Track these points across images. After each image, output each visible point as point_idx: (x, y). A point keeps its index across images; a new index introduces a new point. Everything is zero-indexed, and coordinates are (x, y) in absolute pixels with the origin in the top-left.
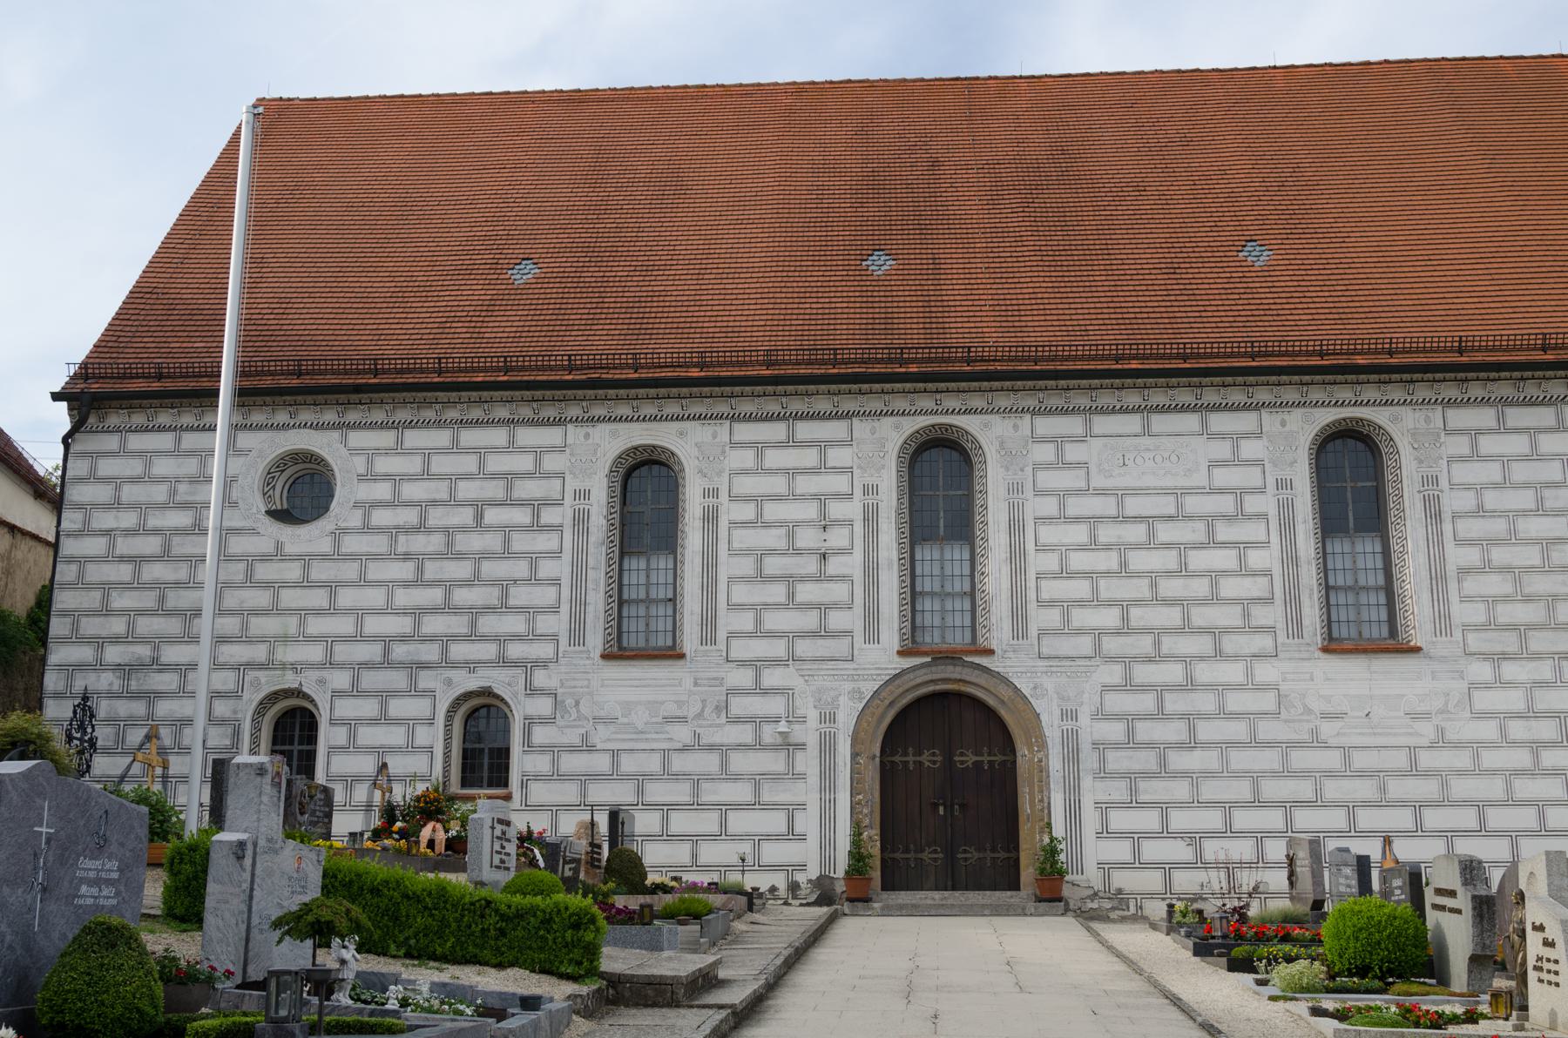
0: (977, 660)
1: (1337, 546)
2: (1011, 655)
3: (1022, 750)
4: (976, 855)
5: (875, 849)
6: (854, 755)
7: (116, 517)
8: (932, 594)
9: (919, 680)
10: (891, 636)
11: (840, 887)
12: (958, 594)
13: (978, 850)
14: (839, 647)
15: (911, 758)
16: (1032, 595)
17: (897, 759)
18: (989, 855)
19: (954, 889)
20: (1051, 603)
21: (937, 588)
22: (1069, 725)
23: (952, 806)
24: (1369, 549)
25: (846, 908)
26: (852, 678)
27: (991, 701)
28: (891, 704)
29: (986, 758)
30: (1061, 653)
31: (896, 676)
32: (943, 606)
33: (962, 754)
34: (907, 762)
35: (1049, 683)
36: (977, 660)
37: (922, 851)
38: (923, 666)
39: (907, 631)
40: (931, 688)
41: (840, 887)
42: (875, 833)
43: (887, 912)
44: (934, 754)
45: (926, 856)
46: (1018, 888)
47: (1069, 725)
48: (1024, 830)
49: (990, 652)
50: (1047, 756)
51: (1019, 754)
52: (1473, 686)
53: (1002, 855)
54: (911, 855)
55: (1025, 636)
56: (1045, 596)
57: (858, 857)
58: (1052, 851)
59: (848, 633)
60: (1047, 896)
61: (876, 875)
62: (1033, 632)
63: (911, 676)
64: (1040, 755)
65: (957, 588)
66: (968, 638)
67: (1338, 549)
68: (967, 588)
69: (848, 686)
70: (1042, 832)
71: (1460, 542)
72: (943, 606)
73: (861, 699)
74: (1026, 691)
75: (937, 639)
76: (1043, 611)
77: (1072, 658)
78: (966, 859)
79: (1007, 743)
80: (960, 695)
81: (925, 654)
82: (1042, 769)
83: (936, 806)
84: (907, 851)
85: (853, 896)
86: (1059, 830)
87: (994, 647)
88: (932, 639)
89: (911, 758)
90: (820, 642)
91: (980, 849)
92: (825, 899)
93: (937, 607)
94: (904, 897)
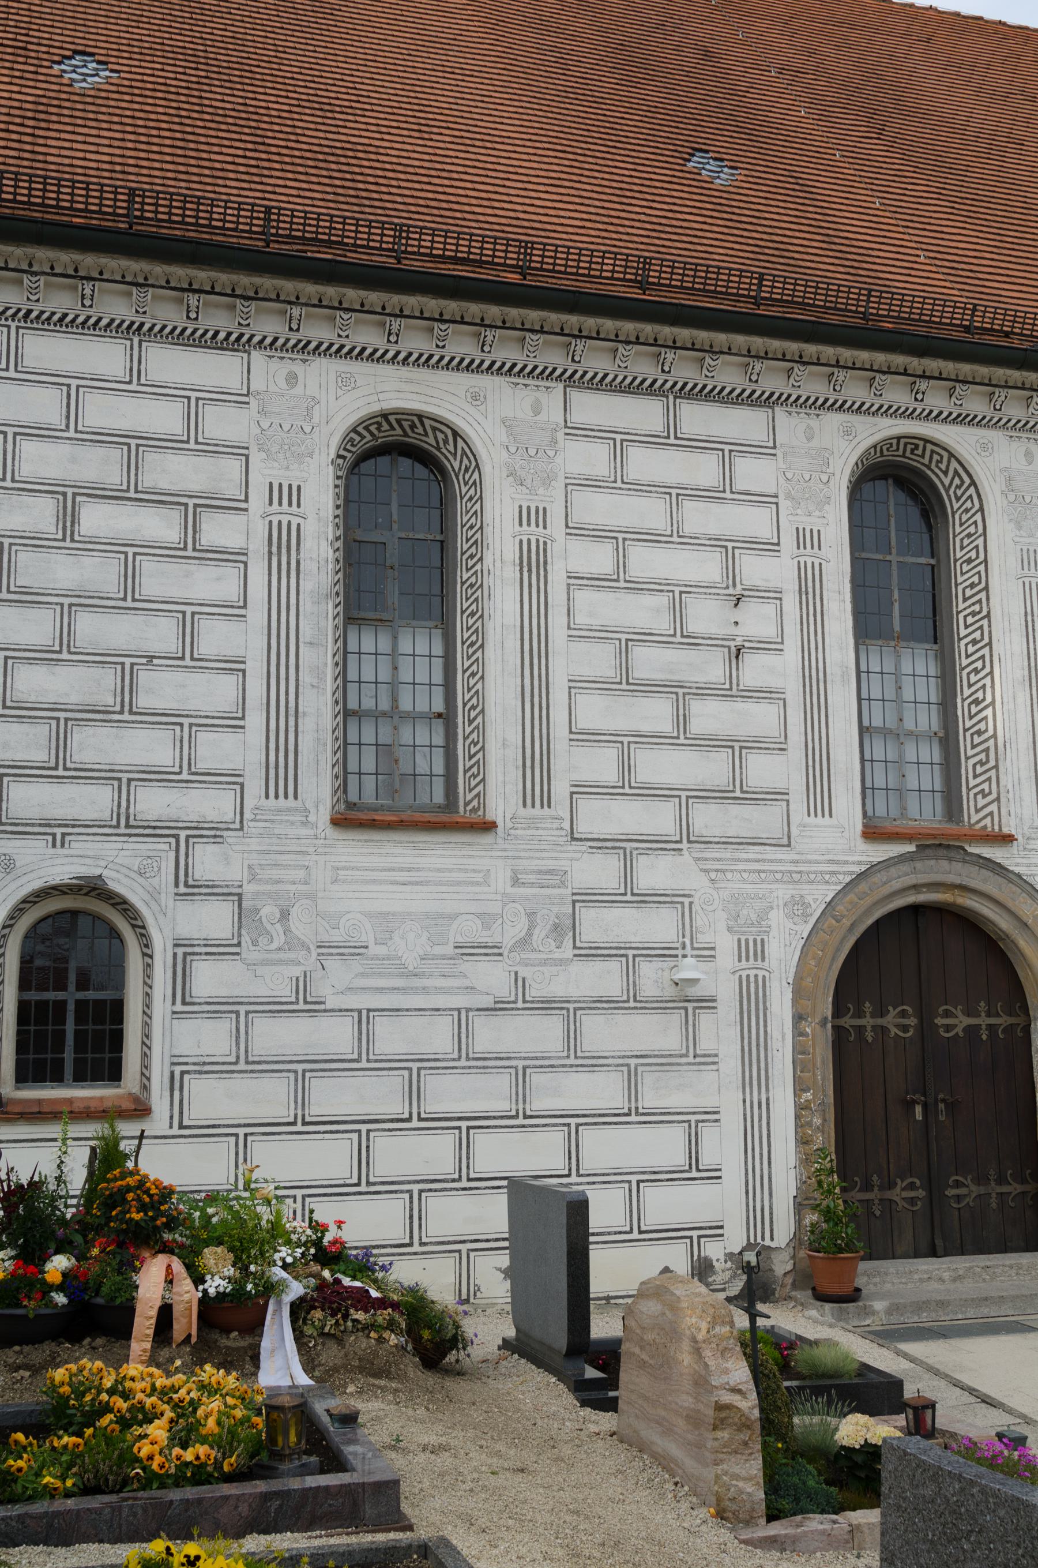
1: (368, 640)
4: (976, 1190)
6: (798, 1018)
9: (896, 885)
11: (781, 1266)
13: (979, 1180)
14: (763, 820)
24: (422, 648)
26: (790, 878)
27: (1004, 923)
28: (853, 926)
31: (861, 876)
33: (947, 1014)
37: (891, 1186)
38: (902, 859)
44: (903, 1014)
49: (1008, 839)
52: (583, 898)
59: (779, 795)
67: (368, 646)
69: (783, 892)
71: (577, 634)
78: (958, 1198)
83: (910, 1105)
90: (734, 809)
91: (981, 1179)
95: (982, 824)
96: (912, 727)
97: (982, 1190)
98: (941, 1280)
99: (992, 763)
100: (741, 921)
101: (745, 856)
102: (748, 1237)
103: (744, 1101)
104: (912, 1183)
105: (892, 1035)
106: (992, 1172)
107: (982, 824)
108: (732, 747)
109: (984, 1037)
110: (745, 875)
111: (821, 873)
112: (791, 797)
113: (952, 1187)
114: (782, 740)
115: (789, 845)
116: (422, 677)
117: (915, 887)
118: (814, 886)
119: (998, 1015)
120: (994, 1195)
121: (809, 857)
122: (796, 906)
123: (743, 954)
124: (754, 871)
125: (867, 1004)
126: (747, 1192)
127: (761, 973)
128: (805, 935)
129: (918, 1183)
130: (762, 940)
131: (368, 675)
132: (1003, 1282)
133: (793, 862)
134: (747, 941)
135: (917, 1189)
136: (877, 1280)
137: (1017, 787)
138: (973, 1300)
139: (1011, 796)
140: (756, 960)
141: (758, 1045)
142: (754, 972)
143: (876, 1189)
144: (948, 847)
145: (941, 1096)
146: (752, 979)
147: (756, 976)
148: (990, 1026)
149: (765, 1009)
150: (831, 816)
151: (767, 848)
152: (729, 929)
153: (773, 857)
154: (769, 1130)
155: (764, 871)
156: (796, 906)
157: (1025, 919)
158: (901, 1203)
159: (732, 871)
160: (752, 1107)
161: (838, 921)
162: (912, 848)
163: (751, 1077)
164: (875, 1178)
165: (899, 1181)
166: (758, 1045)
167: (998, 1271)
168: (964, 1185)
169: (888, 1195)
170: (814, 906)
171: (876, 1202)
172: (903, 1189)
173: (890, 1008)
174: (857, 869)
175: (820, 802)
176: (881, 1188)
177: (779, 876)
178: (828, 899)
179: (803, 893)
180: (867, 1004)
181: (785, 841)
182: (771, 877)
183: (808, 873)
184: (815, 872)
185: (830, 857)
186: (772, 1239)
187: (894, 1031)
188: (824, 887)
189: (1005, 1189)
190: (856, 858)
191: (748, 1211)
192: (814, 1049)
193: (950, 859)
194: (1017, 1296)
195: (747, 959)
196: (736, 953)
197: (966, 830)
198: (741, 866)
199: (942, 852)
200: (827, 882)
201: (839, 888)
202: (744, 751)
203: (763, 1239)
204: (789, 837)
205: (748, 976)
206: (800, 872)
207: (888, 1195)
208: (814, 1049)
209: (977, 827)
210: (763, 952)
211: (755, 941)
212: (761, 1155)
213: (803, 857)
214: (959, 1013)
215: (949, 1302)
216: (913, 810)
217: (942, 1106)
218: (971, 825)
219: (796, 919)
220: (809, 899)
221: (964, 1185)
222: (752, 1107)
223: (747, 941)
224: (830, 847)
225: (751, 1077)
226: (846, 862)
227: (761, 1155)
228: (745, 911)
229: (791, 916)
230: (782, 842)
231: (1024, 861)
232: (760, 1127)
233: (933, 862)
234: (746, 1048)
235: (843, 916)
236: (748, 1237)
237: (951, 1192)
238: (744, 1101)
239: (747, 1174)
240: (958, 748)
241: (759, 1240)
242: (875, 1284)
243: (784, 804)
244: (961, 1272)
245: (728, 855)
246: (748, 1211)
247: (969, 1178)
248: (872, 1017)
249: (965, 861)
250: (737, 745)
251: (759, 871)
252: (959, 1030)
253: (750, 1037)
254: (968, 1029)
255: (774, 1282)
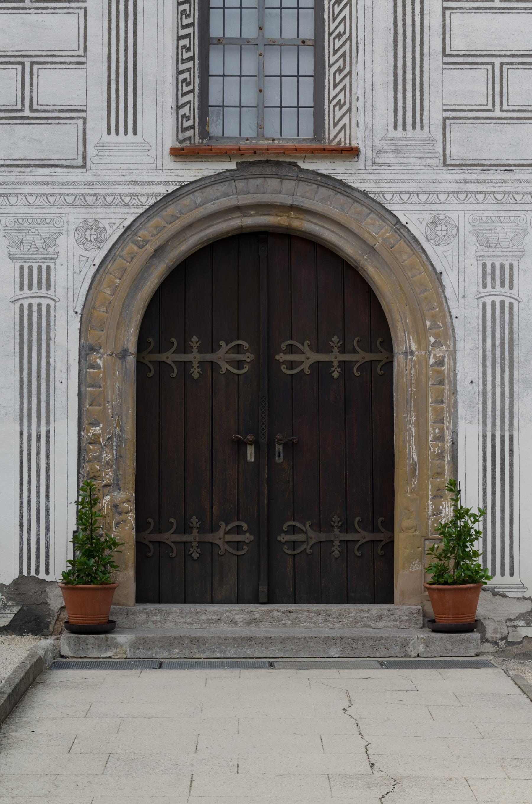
0: (324, 167)
2: (388, 158)
3: (406, 343)
4: (314, 536)
5: (123, 530)
6: (86, 351)
7: (81, 300)
8: (241, 43)
9: (212, 207)
10: (159, 121)
11: (56, 600)
12: (288, 43)
13: (319, 527)
14: (58, 141)
15: (194, 357)
16: (433, 42)
17: (169, 357)
18: (338, 536)
19: (271, 599)
20: (470, 59)
21: (250, 31)
22: (496, 294)
23: (271, 444)
25: (65, 643)
26: (82, 201)
27: (349, 248)
28: (159, 252)
29: (336, 357)
30: (488, 154)
31: (168, 199)
32: (261, 67)
33: (291, 349)
34: (186, 364)
35: (461, 214)
36: (324, 167)
37: (214, 529)
38: (220, 178)
39: (192, 110)
40: (235, 222)
41: (56, 600)
42: (125, 497)
43: (148, 659)
44: (238, 349)
45: (220, 537)
46: (389, 599)
47: (496, 294)
48: (405, 492)
49: (352, 152)
50: (453, 354)
51: (399, 349)
53: (362, 536)
54: (193, 537)
55: (418, 121)
56: (459, 43)
57: (90, 544)
58: (458, 537)
59: (75, 113)
60: (447, 620)
61: (126, 578)
62: (434, 114)
63: (198, 197)
64: (439, 352)
65: (289, 33)
66: (307, 129)
68: (307, 31)
69: (75, 217)
70: (438, 496)
72: (261, 67)
73: (99, 242)
74: (417, 230)
75: (249, 131)
76: (455, 73)
77: (507, 167)
78: (294, 544)
79: (378, 330)
80: (289, 237)
81: (225, 154)
82: (444, 379)
83: (240, 446)
84: (186, 529)
85: (79, 621)
86: (471, 498)
87: (358, 142)
88: (232, 128)
89: (194, 357)
90: (22, 130)
91: (322, 525)
92: (30, 621)
93: (250, 66)
94: (178, 619)
95: (337, 140)
96: (275, 36)
97: (323, 537)
98: (232, 622)
99: (347, 69)
100: (25, 248)
101: (31, 179)
102: (21, 569)
103: (21, 433)
104: (238, 527)
105: (224, 370)
106: (336, 518)
107: (337, 140)
108: (22, 64)
109: (336, 375)
110: (31, 199)
111: (120, 195)
112: (89, 115)
113: (287, 533)
114: (81, 52)
115: (84, 166)
116: (289, 99)
117: (238, 209)
118: (112, 210)
119: (354, 351)
120: (337, 543)
121: (107, 179)
122: (89, 231)
123: (26, 282)
124: (42, 195)
125: (195, 339)
126: (21, 525)
127: (45, 302)
128: (98, 262)
129: (245, 527)
130: (48, 268)
131: (232, 98)
132: (306, 628)
133: (87, 184)
134: (30, 269)
135: (245, 532)
136: (158, 618)
137: (369, 94)
138: (234, 639)
139: (361, 104)
140: (40, 287)
141: (39, 377)
142: (38, 300)
143: (195, 531)
144: (278, 164)
145: (279, 436)
146: (35, 308)
147: (39, 305)
148: (343, 364)
149: (48, 339)
150: (135, 133)
151: (58, 170)
152: (11, 256)
153: (64, 179)
154: (48, 464)
155: (53, 195)
156: (89, 231)
157: (371, 241)
158: (224, 547)
159: (16, 195)
160: (29, 440)
161: (141, 247)
162: (232, 166)
163: (30, 410)
164: (194, 520)
165: (223, 524)
166: (39, 377)
167: (304, 616)
168: (301, 531)
169: (209, 537)
170: (109, 231)
171: (195, 544)
172: (227, 533)
173: (222, 343)
174: (163, 190)
175: (123, 116)
176: (201, 530)
177: (70, 199)
178: (127, 223)
179: (96, 217)
180: (195, 339)
181: (80, 162)
182: (62, 200)
183: (104, 196)
184: (113, 195)
185: (133, 178)
186: (47, 573)
187: (225, 367)
188: (123, 210)
189: (350, 537)
190: (163, 178)
191: (21, 544)
192: (105, 382)
193: (281, 178)
194: (289, 639)
195: (30, 287)
196: (18, 280)
197: (326, 146)
198: (26, 190)
199: (269, 170)
200: (127, 205)
201: (141, 211)
202: (35, 67)
203: (37, 572)
204: (84, 158)
205: (30, 305)
206: (95, 195)
207: (209, 537)
208: (105, 382)
209: (335, 143)
210: (48, 280)
211: (40, 268)
212: (38, 488)
213: (100, 179)
214: (307, 349)
215: (205, 640)
216: (272, 130)
217: (279, 448)
218: (331, 141)
219: (88, 245)
220: (104, 223)
221: (301, 531)
222: (29, 440)
223: (30, 269)
224: (132, 167)
225: (30, 410)
226: (151, 183)
227: (38, 488)
228: (29, 238)
229: (83, 241)
230: (75, 163)
231: (372, 177)
232: (38, 460)
233: (259, 181)
234: (26, 380)
235: (147, 242)
236: (21, 569)
237: (283, 538)
238: (21, 433)
239: (21, 507)
240: (324, 56)
241: (33, 573)
242: (155, 622)
243: (80, 122)
244: (257, 616)
245: (13, 179)
246: (21, 544)
247: (307, 526)
248: (200, 352)
249: (298, 179)
250: (27, 62)
251: (47, 195)
252: (305, 367)
253: (30, 369)
254: (316, 366)
255: (49, 616)
